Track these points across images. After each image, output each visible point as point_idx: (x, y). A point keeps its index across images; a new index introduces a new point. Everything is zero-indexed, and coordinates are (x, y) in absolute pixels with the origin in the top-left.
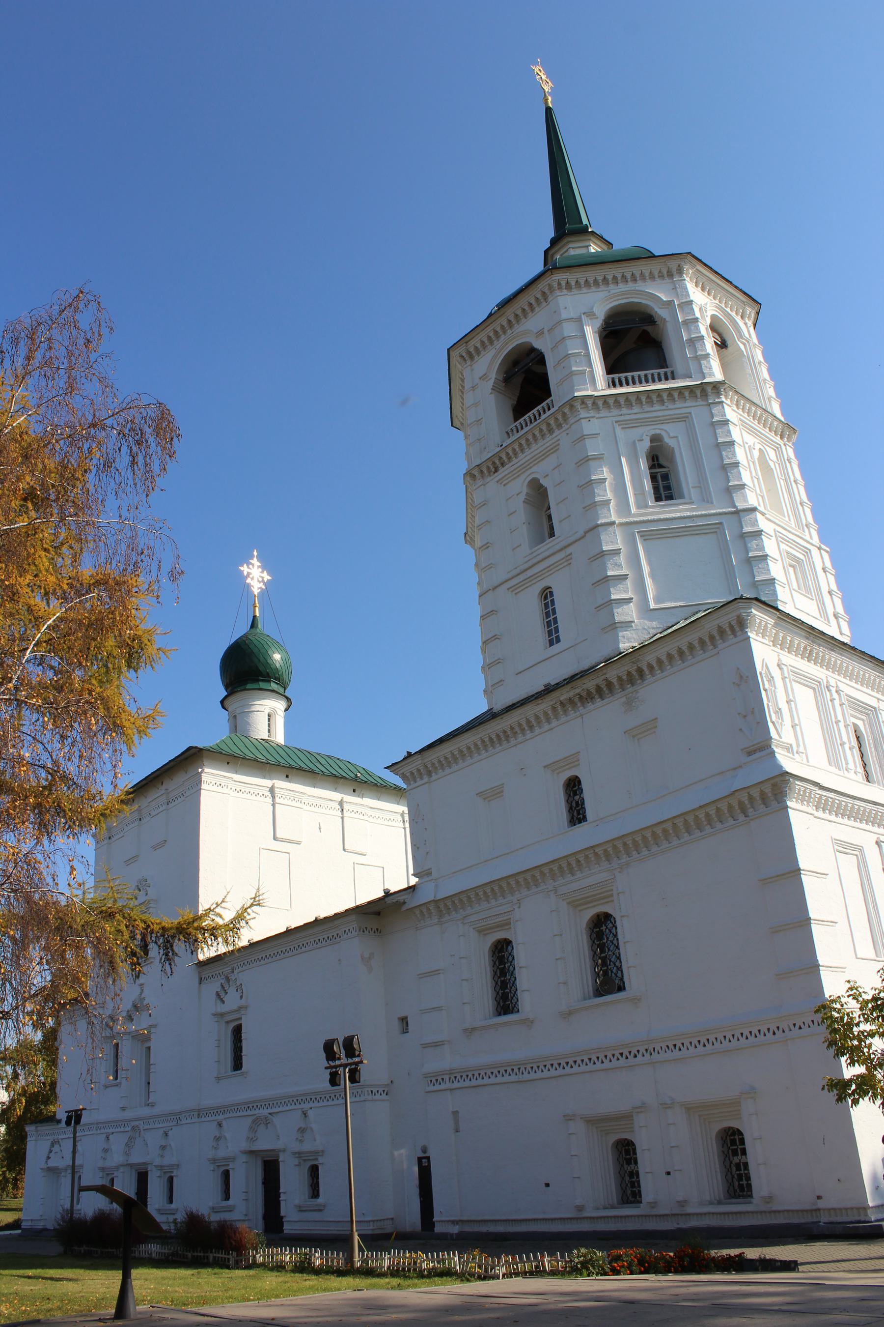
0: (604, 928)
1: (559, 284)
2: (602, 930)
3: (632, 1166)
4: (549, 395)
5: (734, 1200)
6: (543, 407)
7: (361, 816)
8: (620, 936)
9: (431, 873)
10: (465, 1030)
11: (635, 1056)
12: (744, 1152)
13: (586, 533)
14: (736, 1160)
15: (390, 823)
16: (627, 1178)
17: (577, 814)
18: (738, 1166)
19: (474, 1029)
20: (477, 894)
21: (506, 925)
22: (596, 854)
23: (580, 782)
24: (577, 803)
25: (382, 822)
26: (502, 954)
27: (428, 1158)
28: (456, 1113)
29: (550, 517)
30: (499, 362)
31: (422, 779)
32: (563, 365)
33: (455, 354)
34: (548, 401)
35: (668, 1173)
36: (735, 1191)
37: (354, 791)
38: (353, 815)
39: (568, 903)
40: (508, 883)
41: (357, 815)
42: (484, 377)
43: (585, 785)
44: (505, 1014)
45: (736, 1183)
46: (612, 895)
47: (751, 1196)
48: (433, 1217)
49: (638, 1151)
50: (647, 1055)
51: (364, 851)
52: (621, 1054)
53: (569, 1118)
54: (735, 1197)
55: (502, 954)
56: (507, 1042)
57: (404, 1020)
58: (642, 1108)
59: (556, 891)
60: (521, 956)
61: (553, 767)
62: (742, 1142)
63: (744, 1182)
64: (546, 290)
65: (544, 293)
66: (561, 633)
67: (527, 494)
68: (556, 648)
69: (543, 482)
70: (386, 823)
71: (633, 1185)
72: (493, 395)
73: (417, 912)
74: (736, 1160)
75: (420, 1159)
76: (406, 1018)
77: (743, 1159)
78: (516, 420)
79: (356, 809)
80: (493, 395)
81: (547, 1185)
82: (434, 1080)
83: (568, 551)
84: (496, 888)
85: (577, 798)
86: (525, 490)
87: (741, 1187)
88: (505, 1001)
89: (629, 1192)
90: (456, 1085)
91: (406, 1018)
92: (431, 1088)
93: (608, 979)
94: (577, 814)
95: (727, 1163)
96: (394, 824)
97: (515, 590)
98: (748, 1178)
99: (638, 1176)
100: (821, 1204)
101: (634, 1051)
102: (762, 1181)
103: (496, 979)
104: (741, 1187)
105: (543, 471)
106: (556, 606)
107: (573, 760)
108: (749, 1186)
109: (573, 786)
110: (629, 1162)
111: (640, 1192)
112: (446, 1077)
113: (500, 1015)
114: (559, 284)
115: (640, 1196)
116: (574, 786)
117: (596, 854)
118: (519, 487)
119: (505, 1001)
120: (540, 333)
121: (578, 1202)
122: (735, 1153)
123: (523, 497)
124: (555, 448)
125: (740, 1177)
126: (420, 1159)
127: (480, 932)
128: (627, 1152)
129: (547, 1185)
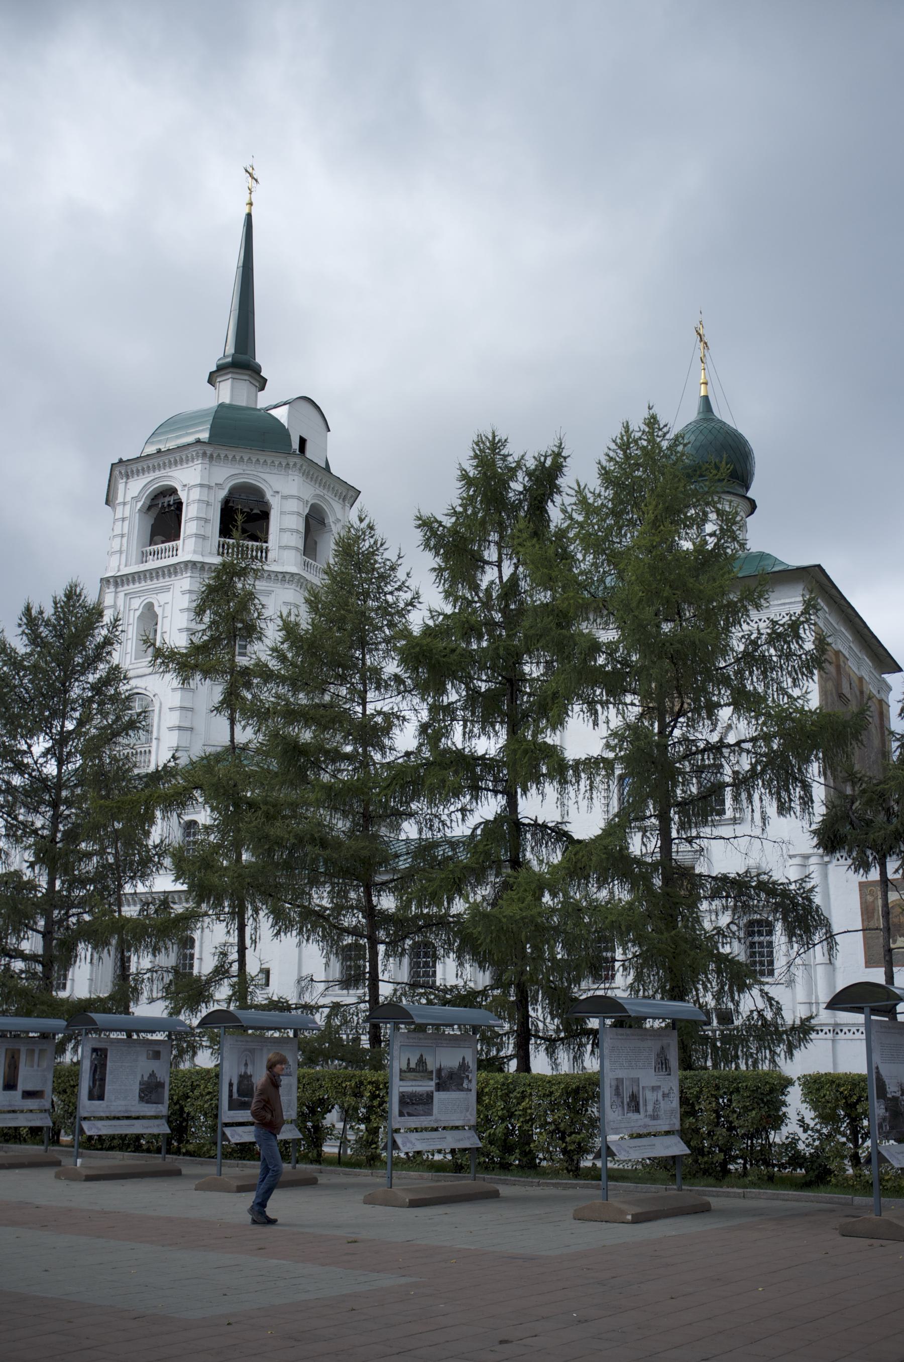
124: (166, 589)
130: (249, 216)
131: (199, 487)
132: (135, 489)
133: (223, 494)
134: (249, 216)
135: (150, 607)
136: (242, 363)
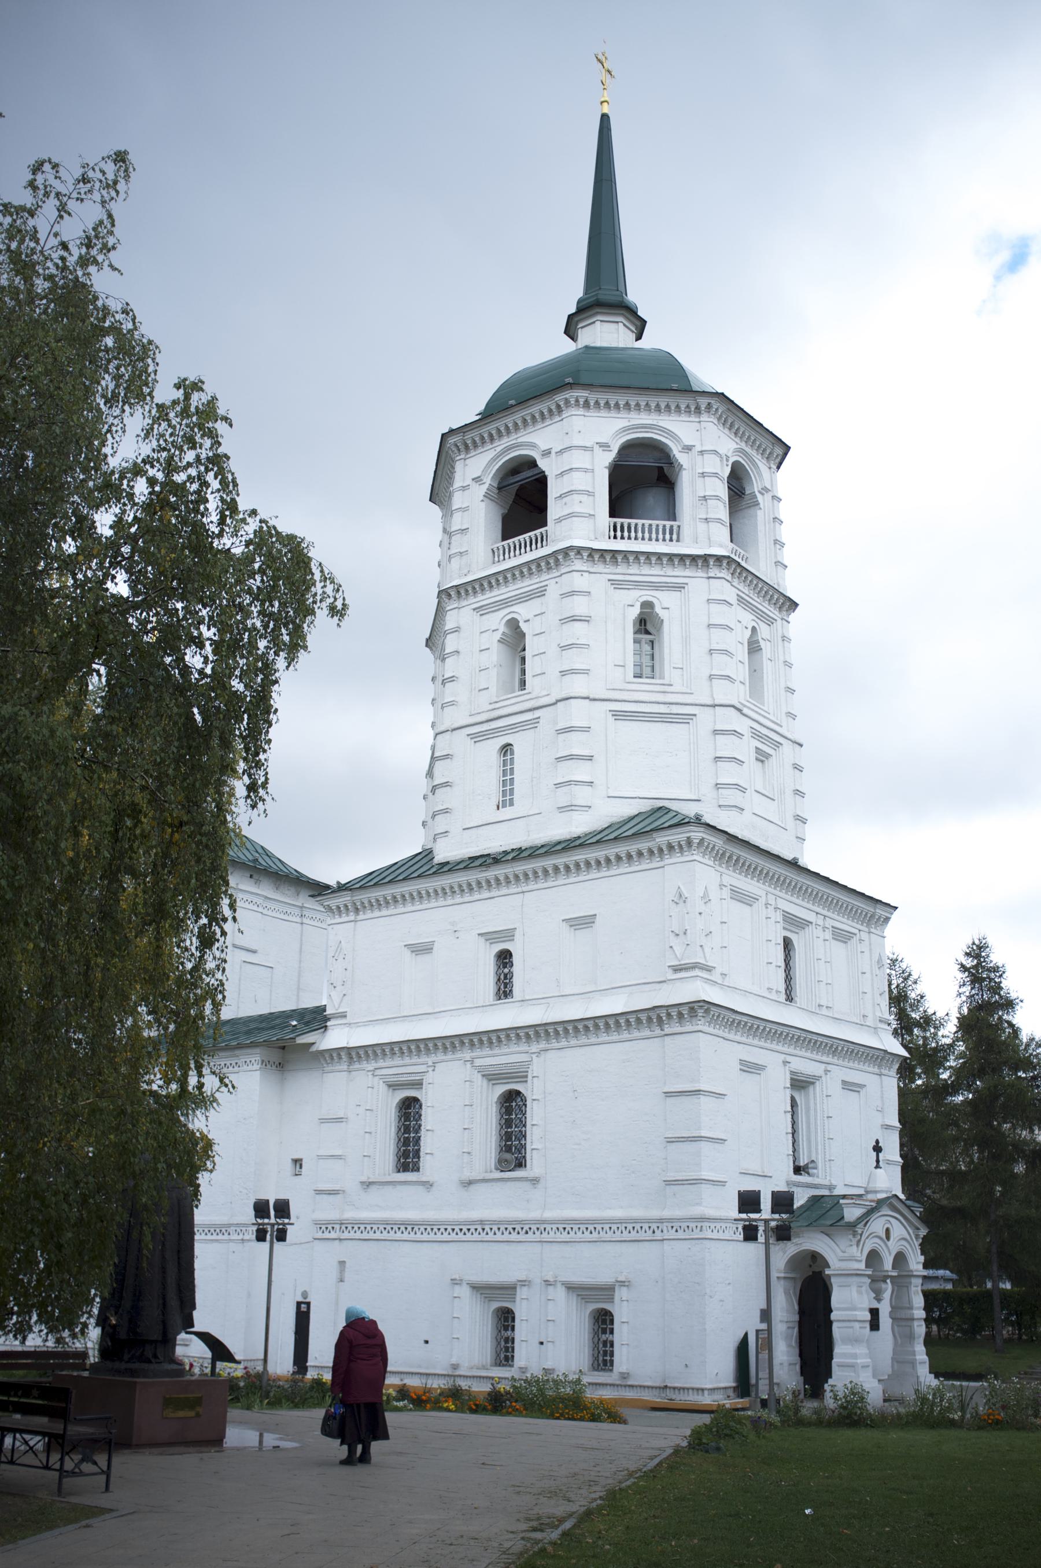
0: (514, 1104)
1: (577, 401)
2: (512, 1104)
3: (509, 1333)
4: (544, 523)
5: (596, 1373)
6: (536, 536)
7: (255, 908)
8: (528, 1115)
9: (345, 1016)
10: (362, 1183)
11: (527, 1233)
12: (612, 1332)
13: (558, 701)
14: (604, 1337)
15: (286, 917)
16: (503, 1343)
17: (504, 989)
18: (605, 1343)
19: (371, 1183)
20: (392, 1049)
21: (418, 1085)
22: (518, 1035)
23: (511, 955)
24: (506, 975)
25: (278, 915)
26: (409, 1111)
27: (308, 1304)
28: (342, 1263)
29: (523, 672)
30: (497, 467)
31: (347, 915)
32: (565, 500)
33: (452, 440)
34: (542, 530)
35: (542, 1343)
36: (599, 1365)
37: (251, 876)
38: (246, 905)
39: (483, 1076)
40: (426, 1045)
41: (251, 906)
42: (477, 480)
43: (515, 959)
44: (404, 1171)
45: (601, 1358)
46: (526, 1076)
47: (611, 1370)
48: (306, 1361)
49: (423, 1107)
50: (538, 1233)
51: (254, 948)
52: (514, 1229)
53: (455, 1282)
54: (597, 1370)
55: (409, 1111)
56: (405, 1202)
57: (298, 1162)
58: (525, 1283)
59: (472, 1062)
60: (429, 1119)
61: (489, 937)
62: (612, 1322)
63: (608, 1358)
64: (562, 403)
65: (558, 406)
66: (516, 797)
67: (504, 634)
68: (507, 813)
69: (523, 626)
70: (282, 916)
71: (507, 1349)
72: (483, 505)
73: (327, 1056)
74: (604, 1337)
75: (299, 1304)
76: (301, 1160)
77: (610, 1338)
78: (504, 539)
79: (250, 898)
80: (483, 505)
81: (427, 1342)
82: (324, 1227)
83: (537, 713)
84: (413, 1047)
85: (506, 970)
86: (502, 628)
87: (605, 1362)
88: (408, 1156)
89: (502, 1356)
90: (346, 1235)
91: (301, 1160)
92: (320, 1235)
93: (512, 1150)
94: (504, 989)
95: (596, 1339)
96: (290, 918)
97: (477, 738)
98: (612, 1354)
99: (513, 1343)
100: (322, 614)
101: (526, 1228)
102: (623, 1359)
103: (400, 1134)
104: (605, 1362)
105: (522, 612)
106: (515, 766)
107: (509, 934)
108: (612, 1362)
109: (504, 958)
110: (506, 1328)
111: (513, 1356)
112: (337, 1227)
113: (399, 1171)
114: (577, 401)
115: (513, 1361)
116: (505, 958)
117: (518, 1035)
118: (497, 621)
119: (408, 1156)
120: (547, 453)
121: (454, 1361)
122: (604, 1332)
123: (498, 635)
124: (541, 593)
125: (605, 1353)
126: (299, 1304)
127: (390, 1086)
128: (506, 1319)
129: (427, 1342)
130: (605, 119)
131: (575, 452)
132: (478, 471)
133: (610, 456)
134: (605, 119)
135: (514, 625)
136: (604, 293)
